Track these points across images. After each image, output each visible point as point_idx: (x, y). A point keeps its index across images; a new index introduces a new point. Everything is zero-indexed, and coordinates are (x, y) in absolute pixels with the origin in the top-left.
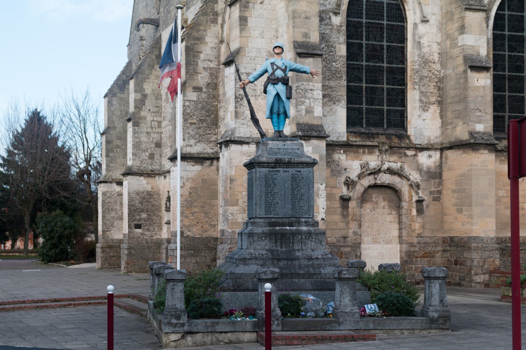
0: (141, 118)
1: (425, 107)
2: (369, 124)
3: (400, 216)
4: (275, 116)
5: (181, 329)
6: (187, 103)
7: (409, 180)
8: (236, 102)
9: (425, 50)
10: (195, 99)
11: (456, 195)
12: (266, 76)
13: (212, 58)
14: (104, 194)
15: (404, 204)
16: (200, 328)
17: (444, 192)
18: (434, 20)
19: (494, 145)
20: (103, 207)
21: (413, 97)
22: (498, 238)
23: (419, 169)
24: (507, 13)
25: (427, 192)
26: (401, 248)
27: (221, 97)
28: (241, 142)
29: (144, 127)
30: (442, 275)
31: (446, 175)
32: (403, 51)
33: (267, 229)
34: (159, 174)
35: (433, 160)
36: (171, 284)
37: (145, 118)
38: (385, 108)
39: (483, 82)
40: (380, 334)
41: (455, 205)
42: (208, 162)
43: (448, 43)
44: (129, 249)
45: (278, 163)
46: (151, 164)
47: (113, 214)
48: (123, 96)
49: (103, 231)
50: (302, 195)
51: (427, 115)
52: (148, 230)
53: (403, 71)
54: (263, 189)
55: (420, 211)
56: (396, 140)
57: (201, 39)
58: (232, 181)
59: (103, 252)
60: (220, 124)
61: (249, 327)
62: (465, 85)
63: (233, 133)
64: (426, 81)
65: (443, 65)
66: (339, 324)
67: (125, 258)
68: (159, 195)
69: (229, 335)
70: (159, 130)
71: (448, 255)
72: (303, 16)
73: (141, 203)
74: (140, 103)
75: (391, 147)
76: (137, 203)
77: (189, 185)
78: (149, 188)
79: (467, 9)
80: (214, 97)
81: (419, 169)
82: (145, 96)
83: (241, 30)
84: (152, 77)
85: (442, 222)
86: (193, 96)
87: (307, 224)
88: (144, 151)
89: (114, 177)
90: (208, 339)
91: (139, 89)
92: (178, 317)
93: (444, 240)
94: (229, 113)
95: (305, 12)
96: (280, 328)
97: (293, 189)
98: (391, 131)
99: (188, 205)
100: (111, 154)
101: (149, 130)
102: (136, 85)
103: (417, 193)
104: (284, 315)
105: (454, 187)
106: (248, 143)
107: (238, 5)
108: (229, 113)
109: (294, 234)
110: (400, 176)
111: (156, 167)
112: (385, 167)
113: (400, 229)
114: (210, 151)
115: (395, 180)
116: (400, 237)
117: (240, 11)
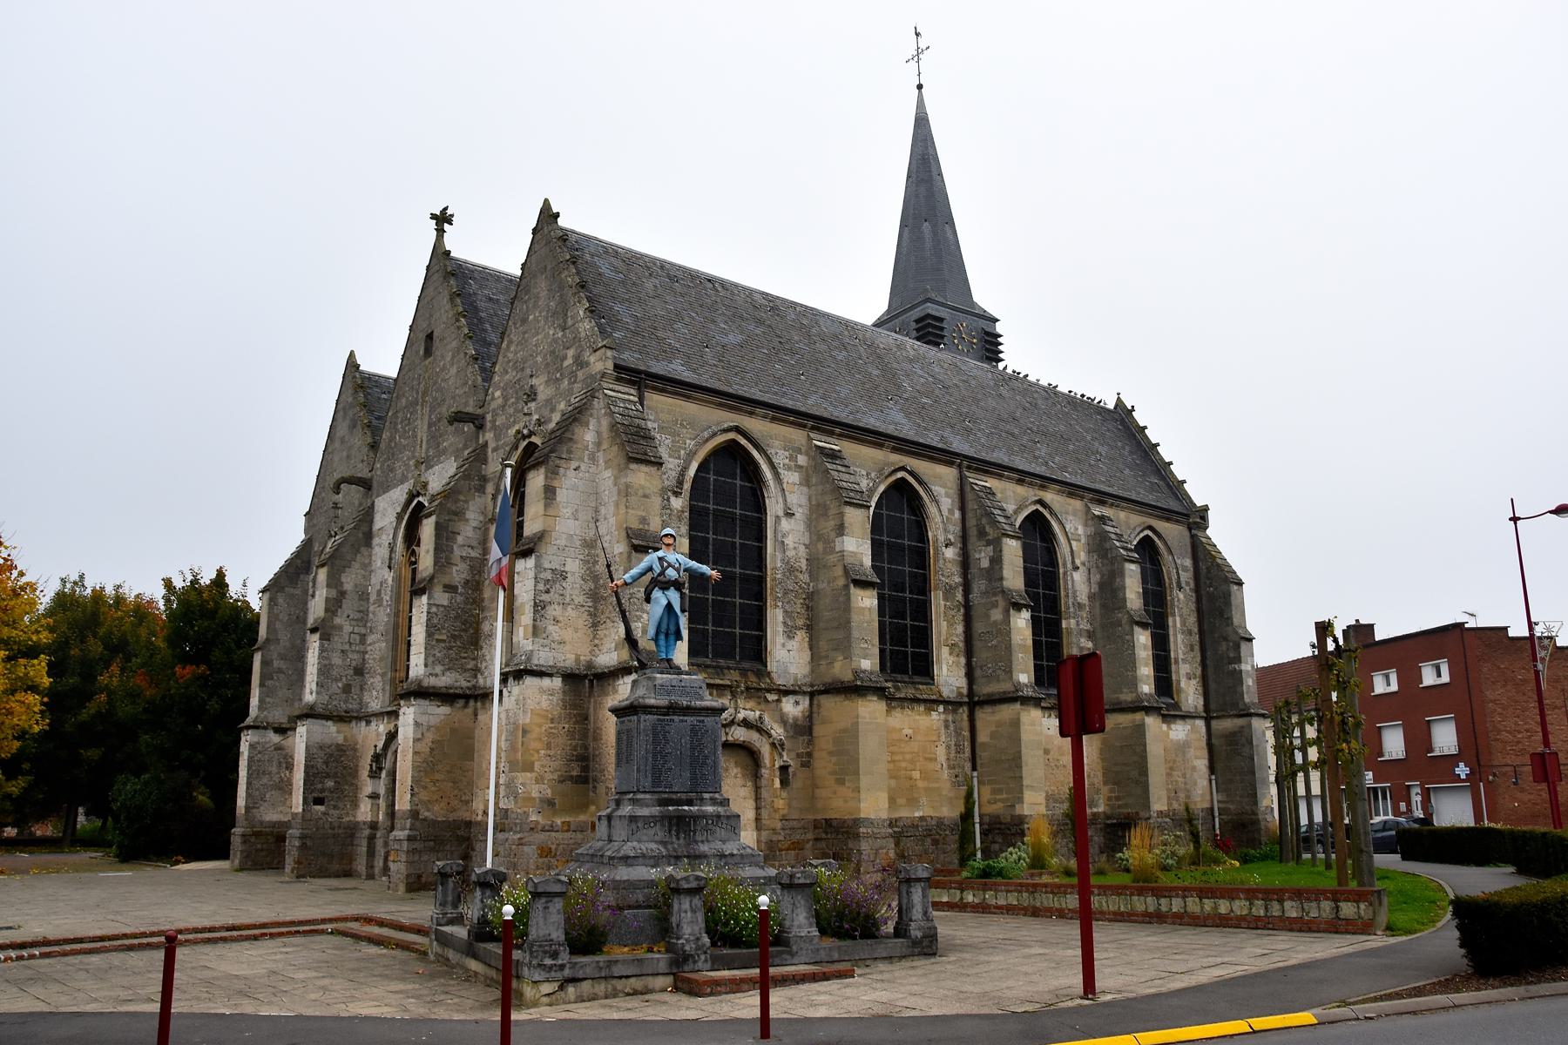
0: (334, 627)
1: (790, 635)
2: (716, 655)
3: (757, 789)
4: (662, 637)
5: (559, 975)
6: (434, 609)
7: (770, 736)
8: (535, 612)
9: (790, 553)
10: (446, 603)
11: (834, 759)
12: (649, 576)
13: (475, 544)
14: (252, 746)
15: (765, 772)
16: (589, 971)
17: (816, 755)
18: (800, 513)
19: (883, 689)
20: (249, 767)
21: (775, 618)
22: (892, 823)
23: (783, 720)
24: (884, 512)
25: (793, 755)
26: (759, 836)
27: (486, 603)
28: (540, 674)
29: (338, 642)
30: (925, 875)
31: (818, 730)
32: (760, 553)
33: (656, 810)
34: (359, 719)
35: (800, 708)
36: (543, 900)
37: (340, 628)
38: (738, 631)
39: (866, 601)
40: (858, 971)
41: (833, 773)
42: (461, 702)
43: (820, 546)
44: (302, 837)
45: (673, 709)
46: (346, 702)
47: (265, 780)
48: (298, 592)
49: (247, 808)
50: (706, 757)
51: (794, 644)
52: (335, 807)
53: (761, 581)
54: (650, 747)
55: (785, 783)
56: (753, 678)
57: (459, 514)
58: (525, 732)
59: (244, 842)
60: (481, 643)
61: (663, 967)
62: (846, 606)
63: (529, 659)
64: (791, 596)
65: (813, 575)
66: (793, 955)
67: (295, 853)
68: (355, 750)
69: (632, 980)
70: (362, 648)
71: (823, 845)
72: (640, 493)
73: (326, 763)
74: (333, 606)
75: (748, 689)
76: (320, 764)
77: (430, 736)
78: (340, 739)
79: (847, 503)
80: (474, 601)
81: (783, 720)
82: (343, 594)
83: (546, 506)
84: (356, 565)
85: (813, 797)
86: (442, 598)
87: (714, 802)
88: (337, 680)
89: (270, 720)
90: (601, 988)
91: (334, 581)
92: (555, 955)
93: (816, 825)
94: (521, 629)
95: (643, 487)
96: (709, 965)
97: (693, 748)
98: (746, 665)
99: (426, 768)
100: (269, 683)
101: (347, 647)
102: (330, 576)
103: (781, 756)
104: (713, 944)
105: (831, 747)
106: (550, 675)
107: (542, 470)
108: (521, 629)
109: (696, 818)
110: (760, 730)
111: (353, 706)
112: (741, 716)
113: (758, 808)
114: (464, 684)
115: (752, 737)
116: (758, 819)
117: (546, 477)
